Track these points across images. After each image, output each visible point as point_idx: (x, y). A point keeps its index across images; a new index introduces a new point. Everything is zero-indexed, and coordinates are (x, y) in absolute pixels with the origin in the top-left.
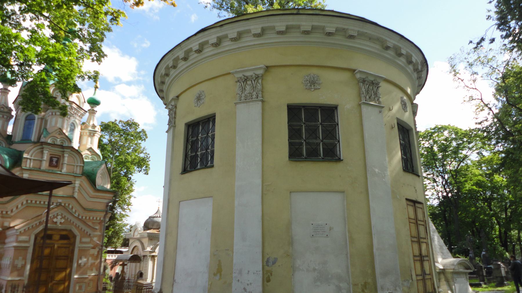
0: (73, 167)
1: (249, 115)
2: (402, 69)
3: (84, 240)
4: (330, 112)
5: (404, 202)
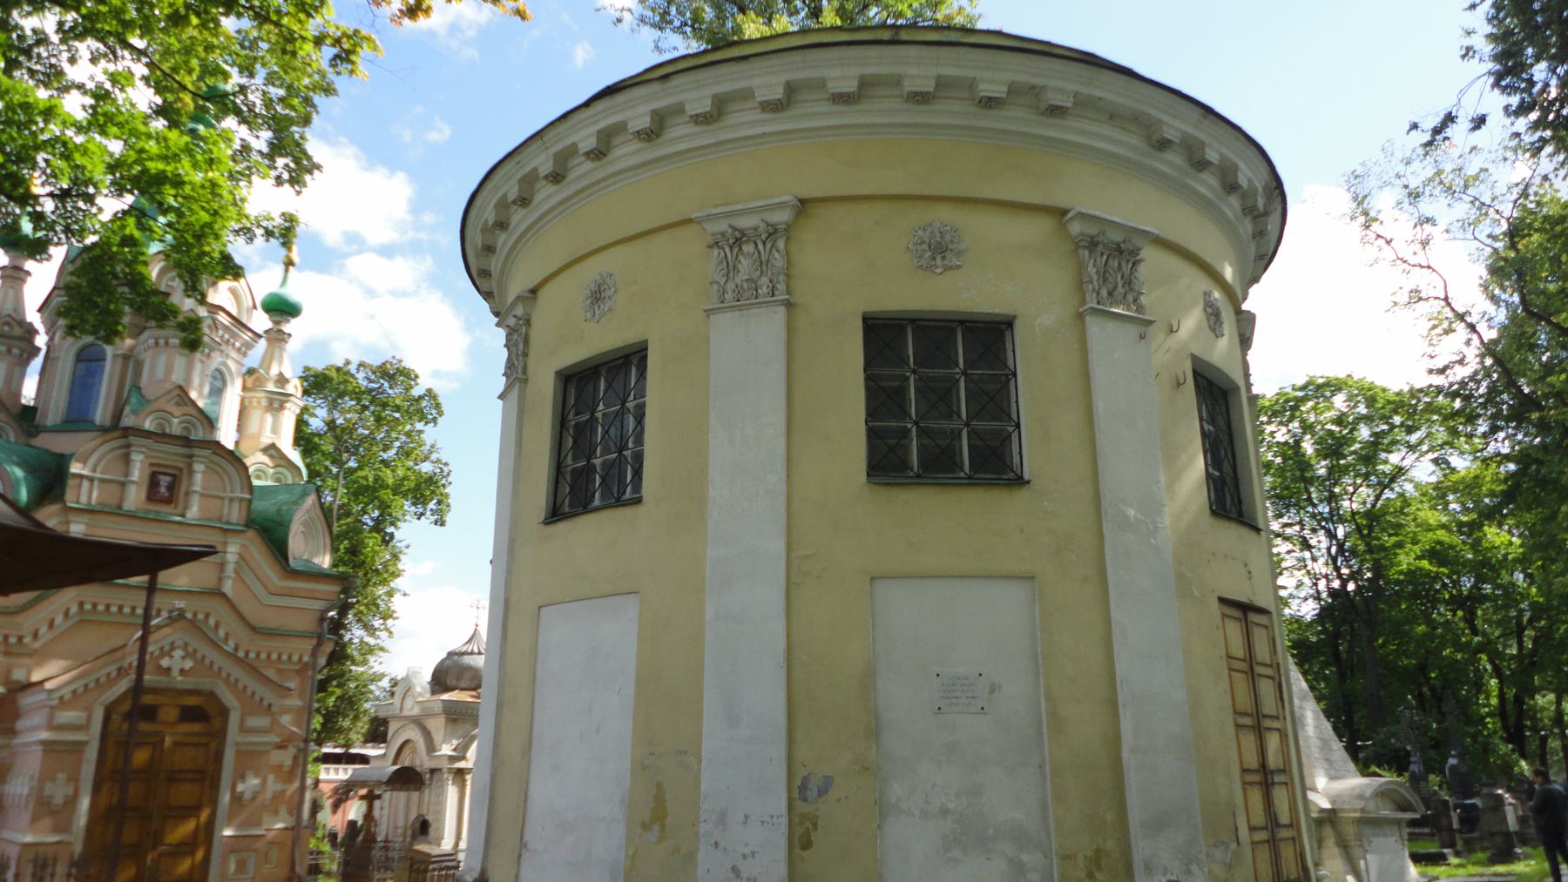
0: (218, 502)
1: (748, 346)
2: (1207, 207)
3: (252, 722)
4: (990, 336)
5: (1215, 608)
